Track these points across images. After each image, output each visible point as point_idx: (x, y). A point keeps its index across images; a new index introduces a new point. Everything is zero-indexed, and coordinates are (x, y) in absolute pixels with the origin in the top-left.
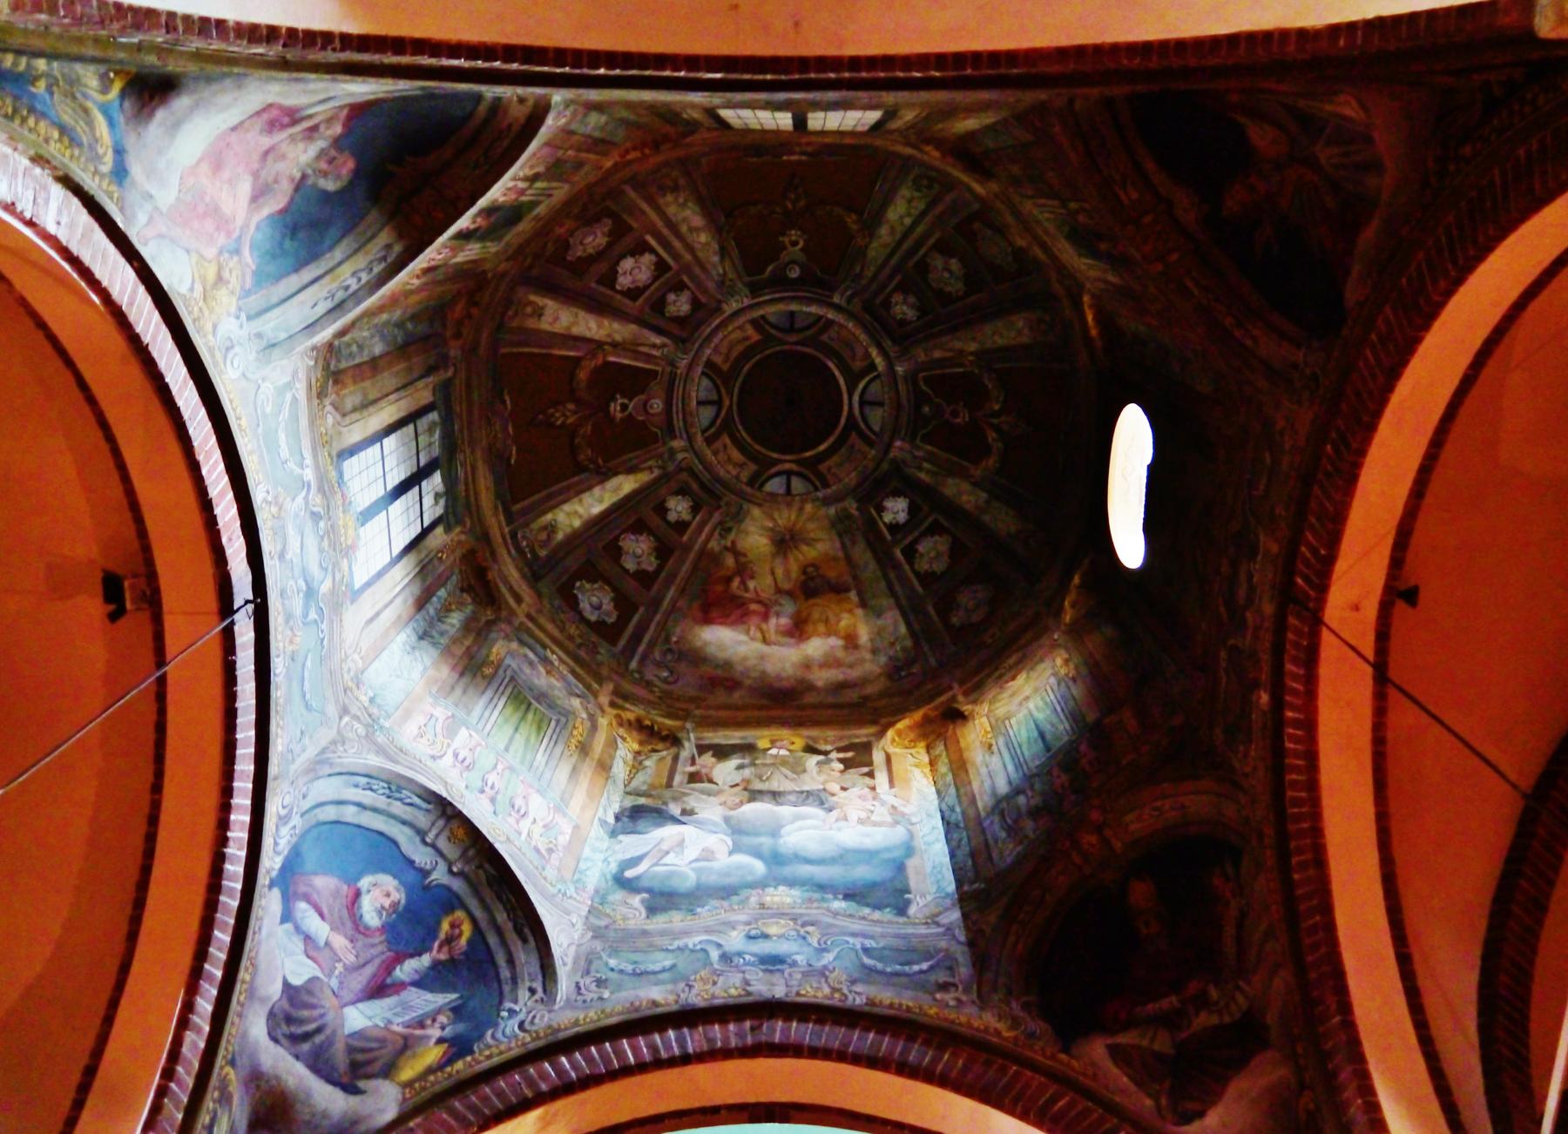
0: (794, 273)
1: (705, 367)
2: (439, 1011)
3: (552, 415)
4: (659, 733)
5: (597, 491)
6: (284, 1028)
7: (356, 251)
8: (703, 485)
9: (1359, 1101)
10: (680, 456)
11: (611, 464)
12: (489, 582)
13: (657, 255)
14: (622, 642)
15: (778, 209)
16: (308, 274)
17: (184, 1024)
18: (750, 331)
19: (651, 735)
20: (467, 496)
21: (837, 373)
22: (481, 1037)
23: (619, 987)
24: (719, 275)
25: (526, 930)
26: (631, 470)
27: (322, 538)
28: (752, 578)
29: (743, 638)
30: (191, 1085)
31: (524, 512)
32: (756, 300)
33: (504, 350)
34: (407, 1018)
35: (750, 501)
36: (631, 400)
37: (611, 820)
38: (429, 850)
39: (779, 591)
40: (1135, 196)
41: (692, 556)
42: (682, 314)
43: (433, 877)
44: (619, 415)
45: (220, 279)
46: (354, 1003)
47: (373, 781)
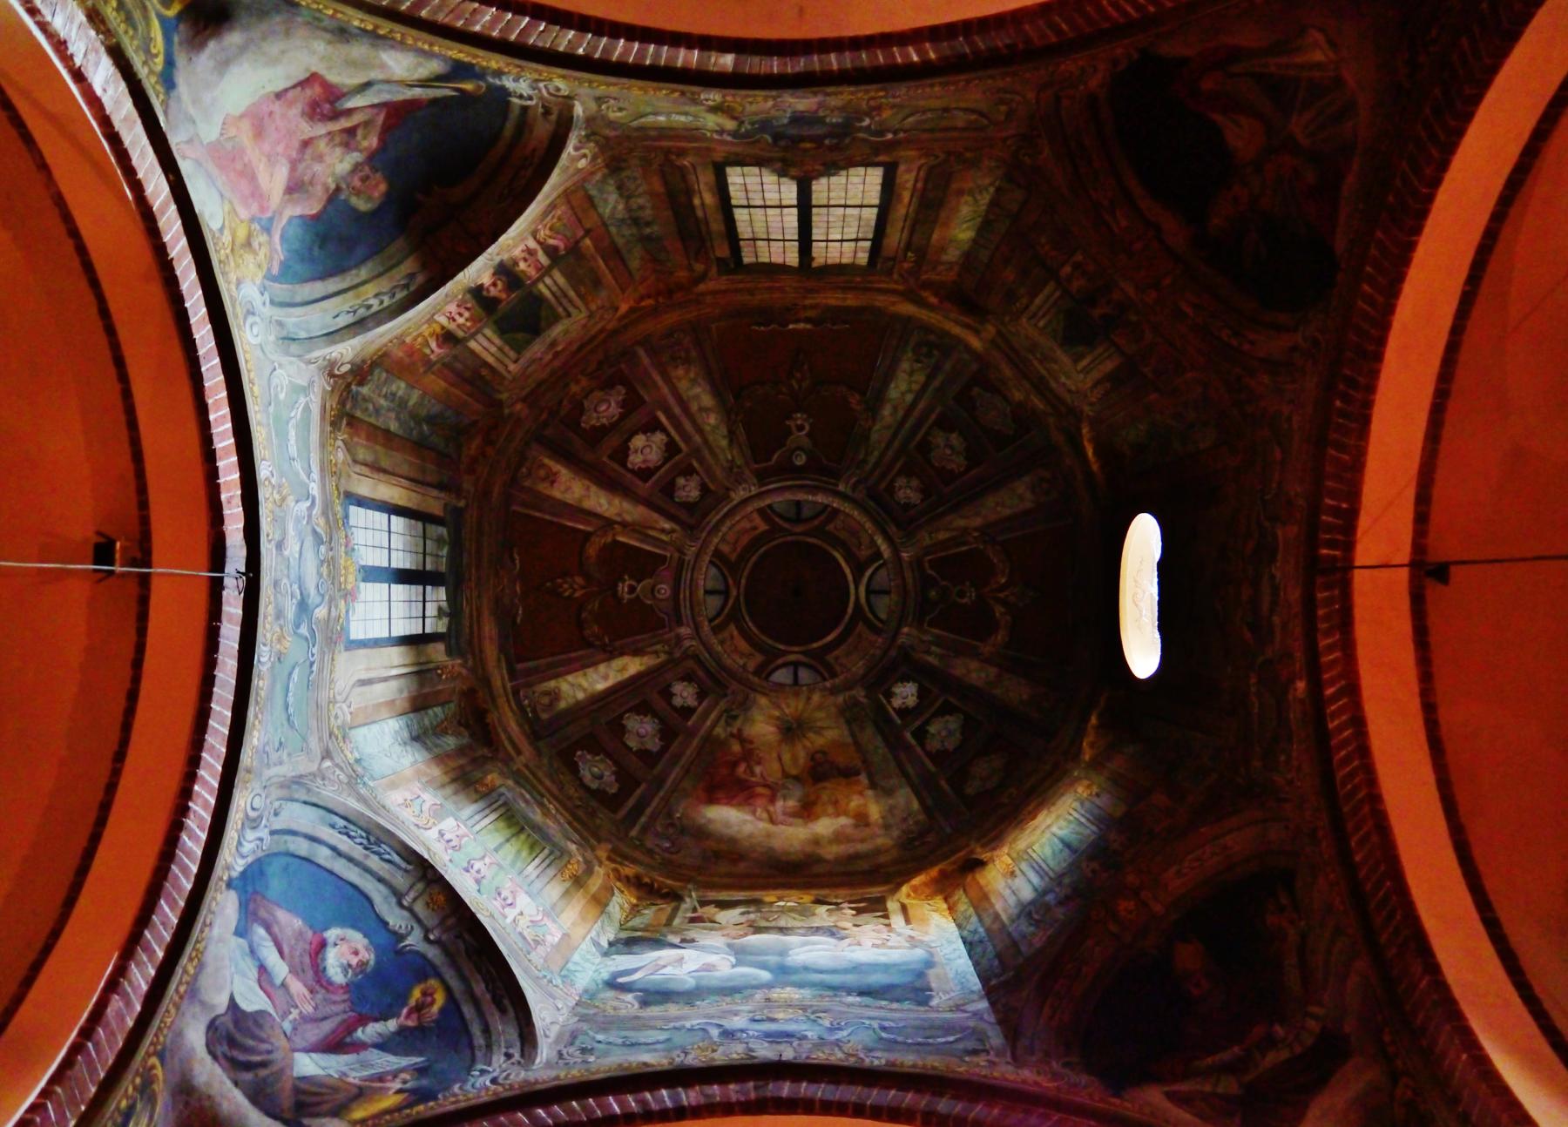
0: (800, 460)
1: (713, 555)
2: (403, 1070)
3: (561, 586)
4: (659, 891)
5: (602, 668)
6: (225, 1048)
7: (380, 275)
8: (708, 672)
9: (1464, 1056)
10: (687, 643)
11: (617, 644)
12: (488, 725)
13: (668, 435)
14: (622, 813)
15: (784, 390)
16: (333, 285)
17: (113, 986)
18: (758, 521)
19: (647, 891)
20: (471, 633)
21: (843, 564)
22: (448, 1088)
23: (606, 1054)
24: (728, 461)
25: (506, 1002)
26: (637, 652)
27: (322, 562)
28: (759, 763)
29: (749, 817)
30: (110, 1062)
31: (528, 673)
32: (764, 489)
33: (515, 508)
34: (365, 1073)
35: (755, 690)
36: (639, 582)
37: (606, 945)
38: (406, 914)
39: (786, 775)
40: (1124, 223)
41: (695, 742)
42: (691, 500)
43: (407, 942)
44: (627, 596)
45: (248, 244)
46: (307, 1050)
47: (352, 827)
